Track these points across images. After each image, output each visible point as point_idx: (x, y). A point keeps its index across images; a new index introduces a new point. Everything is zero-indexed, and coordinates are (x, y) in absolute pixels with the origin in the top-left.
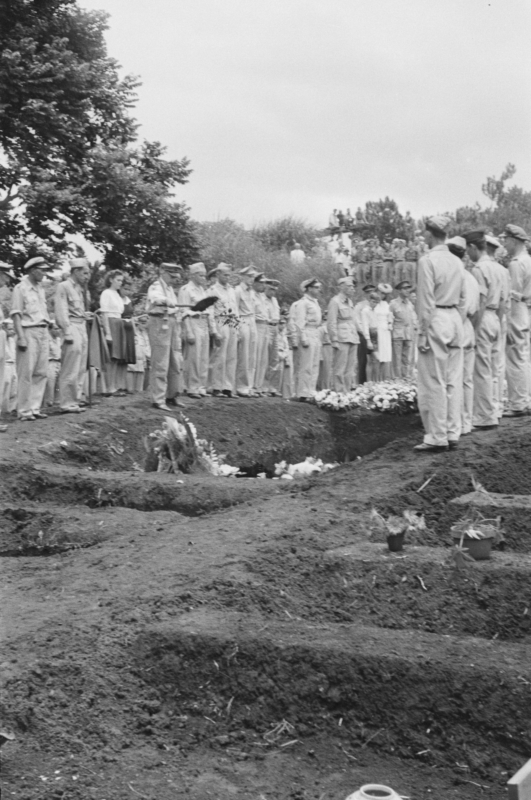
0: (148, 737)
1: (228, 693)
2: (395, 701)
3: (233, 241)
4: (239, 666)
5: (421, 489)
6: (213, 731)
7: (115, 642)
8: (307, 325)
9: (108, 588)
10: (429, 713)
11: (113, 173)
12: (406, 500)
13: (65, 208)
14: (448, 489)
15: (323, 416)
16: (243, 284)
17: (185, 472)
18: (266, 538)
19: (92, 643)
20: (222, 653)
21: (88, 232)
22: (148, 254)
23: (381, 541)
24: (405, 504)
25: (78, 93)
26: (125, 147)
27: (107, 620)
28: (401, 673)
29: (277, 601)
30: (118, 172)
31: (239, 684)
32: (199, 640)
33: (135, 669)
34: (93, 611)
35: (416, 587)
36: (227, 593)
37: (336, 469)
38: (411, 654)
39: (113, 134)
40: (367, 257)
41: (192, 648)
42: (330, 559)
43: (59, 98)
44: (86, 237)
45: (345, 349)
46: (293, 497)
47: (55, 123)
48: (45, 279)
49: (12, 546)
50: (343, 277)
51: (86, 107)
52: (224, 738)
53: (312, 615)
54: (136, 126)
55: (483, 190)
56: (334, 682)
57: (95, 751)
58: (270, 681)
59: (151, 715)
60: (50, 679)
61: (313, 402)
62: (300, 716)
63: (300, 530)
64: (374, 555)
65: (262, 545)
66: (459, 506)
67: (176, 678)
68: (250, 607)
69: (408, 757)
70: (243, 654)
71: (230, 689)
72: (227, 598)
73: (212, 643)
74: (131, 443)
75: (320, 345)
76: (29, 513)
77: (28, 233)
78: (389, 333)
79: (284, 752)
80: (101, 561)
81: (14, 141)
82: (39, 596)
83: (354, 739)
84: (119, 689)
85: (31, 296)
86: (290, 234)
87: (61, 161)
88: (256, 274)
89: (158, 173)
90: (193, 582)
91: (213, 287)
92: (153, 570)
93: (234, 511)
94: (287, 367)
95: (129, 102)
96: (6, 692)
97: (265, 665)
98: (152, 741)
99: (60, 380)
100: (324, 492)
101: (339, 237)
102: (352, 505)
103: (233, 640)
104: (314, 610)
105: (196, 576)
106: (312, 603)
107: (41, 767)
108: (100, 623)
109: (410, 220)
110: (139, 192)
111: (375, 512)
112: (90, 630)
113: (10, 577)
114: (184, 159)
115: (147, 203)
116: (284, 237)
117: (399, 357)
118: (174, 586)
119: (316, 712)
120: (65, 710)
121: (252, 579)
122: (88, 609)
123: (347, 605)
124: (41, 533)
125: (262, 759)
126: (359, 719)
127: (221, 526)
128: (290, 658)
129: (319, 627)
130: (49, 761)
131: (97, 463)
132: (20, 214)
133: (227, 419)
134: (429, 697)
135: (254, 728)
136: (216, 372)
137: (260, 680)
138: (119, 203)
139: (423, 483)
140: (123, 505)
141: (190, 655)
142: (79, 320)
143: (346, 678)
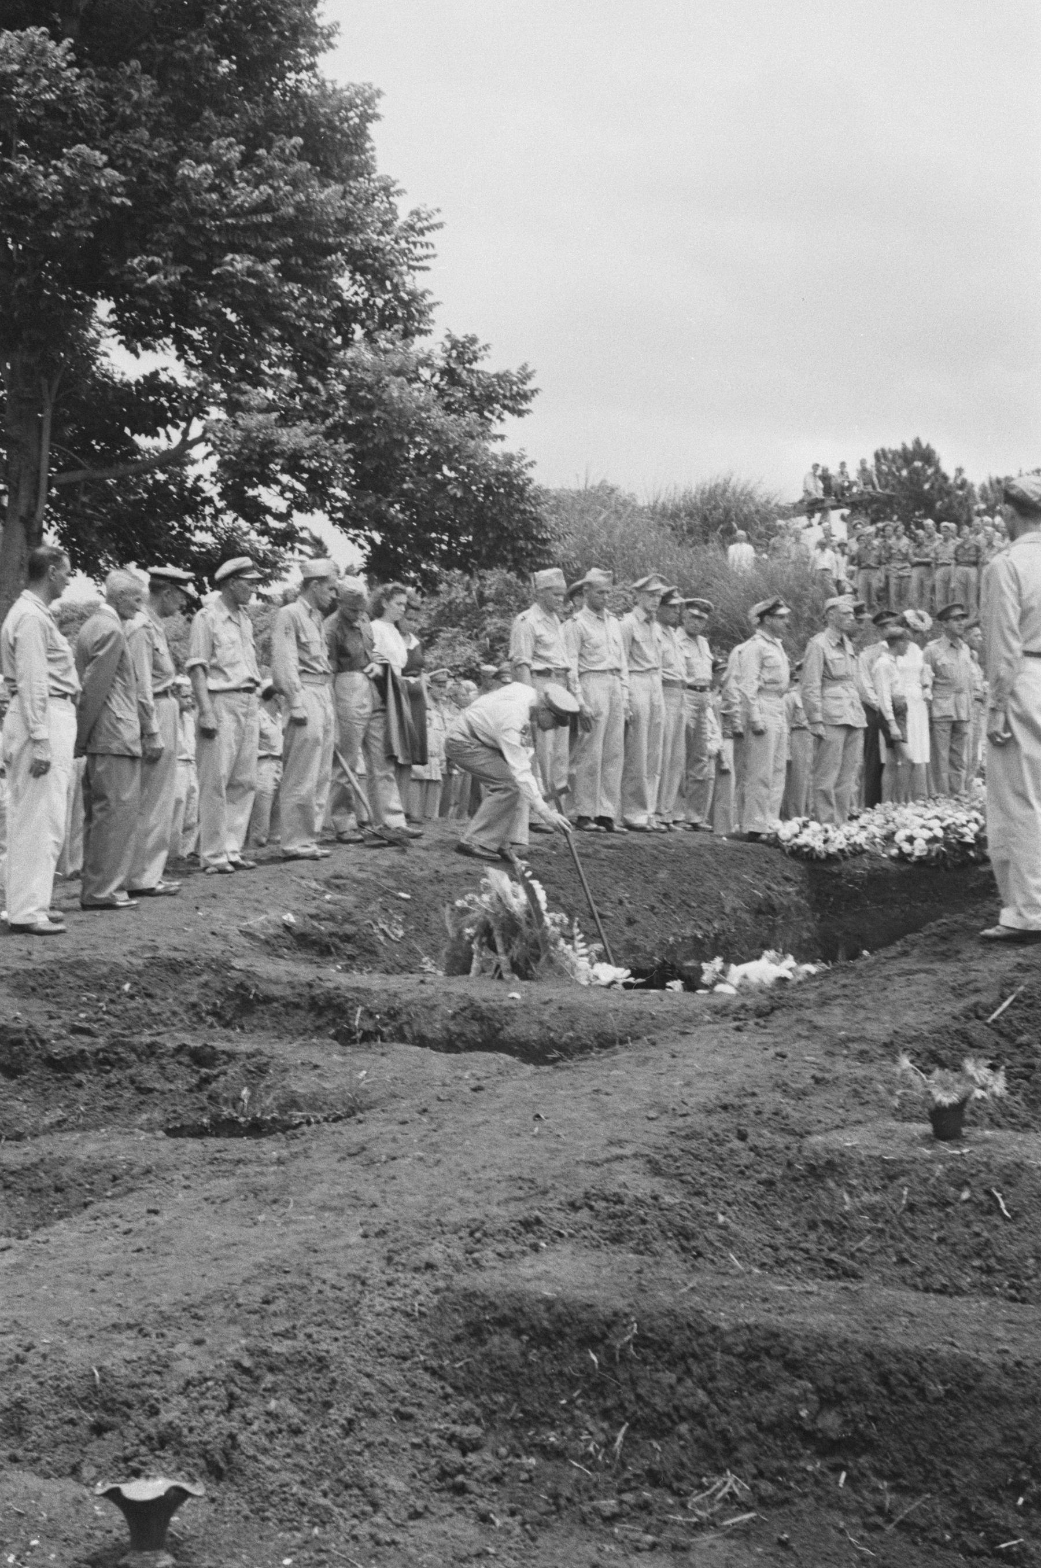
0: (458, 1499)
1: (617, 1416)
2: (953, 1439)
3: (614, 526)
4: (638, 1362)
5: (994, 1016)
6: (586, 1490)
7: (394, 1309)
8: (760, 690)
9: (379, 1203)
10: (1021, 1464)
11: (385, 396)
12: (964, 1036)
13: (293, 464)
15: (794, 869)
16: (637, 610)
17: (524, 977)
18: (685, 1109)
19: (351, 1309)
20: (605, 1336)
21: (335, 510)
22: (450, 552)
23: (919, 1120)
24: (964, 1046)
25: (320, 244)
26: (408, 346)
27: (377, 1264)
28: (964, 1383)
29: (711, 1234)
30: (395, 394)
31: (639, 1397)
32: (560, 1308)
33: (434, 1363)
34: (349, 1248)
35: (989, 1212)
36: (613, 1216)
37: (824, 975)
38: (984, 1345)
39: (386, 321)
40: (879, 557)
41: (546, 1323)
42: (815, 1153)
43: (284, 253)
44: (331, 519)
45: (839, 737)
46: (738, 1029)
47: (277, 301)
48: (254, 601)
49: (191, 1117)
50: (832, 596)
51: (334, 269)
52: (609, 1505)
53: (780, 1263)
54: (431, 307)
56: (828, 1400)
57: (355, 1521)
58: (701, 1394)
59: (464, 1454)
60: (269, 1379)
61: (775, 842)
62: (762, 1466)
63: (754, 1094)
64: (904, 1147)
65: (679, 1122)
67: (515, 1383)
68: (657, 1246)
69: (979, 1554)
70: (646, 1338)
71: (621, 1407)
72: (611, 1227)
73: (584, 1316)
74: (419, 918)
75: (786, 730)
76: (224, 1052)
77: (219, 511)
78: (924, 706)
79: (729, 1536)
80: (364, 1149)
81: (196, 334)
82: (244, 1216)
83: (870, 1514)
84: (403, 1401)
85: (227, 633)
86: (727, 512)
87: (286, 373)
88: (665, 589)
89: (472, 395)
90: (545, 1192)
91: (577, 615)
92: (465, 1167)
93: (623, 1054)
94: (723, 773)
96: (185, 1403)
97: (690, 1361)
98: (468, 1507)
99: (281, 795)
100: (799, 1021)
101: (825, 517)
102: (856, 1047)
103: (627, 1310)
104: (785, 1253)
105: (549, 1183)
106: (780, 1239)
107: (255, 1551)
108: (365, 1270)
109: (963, 485)
110: (436, 432)
111: (905, 1062)
112: (344, 1283)
113: (187, 1178)
114: (524, 368)
115: (450, 453)
116: (715, 518)
117: (945, 753)
118: (507, 1201)
119: (792, 1458)
120: (298, 1440)
121: (660, 1190)
122: (341, 1242)
123: (851, 1246)
124: (245, 1092)
125: (685, 1549)
126: (880, 1474)
127: (596, 1084)
128: (741, 1349)
129: (798, 1287)
130: (269, 1538)
131: (352, 958)
132: (207, 476)
133: (604, 874)
134: (1022, 1432)
135: (669, 1487)
136: (583, 782)
137: (681, 1390)
138: (397, 454)
139: (1000, 1004)
140: (403, 1039)
141: (542, 1338)
142: (318, 679)
143: (853, 1391)
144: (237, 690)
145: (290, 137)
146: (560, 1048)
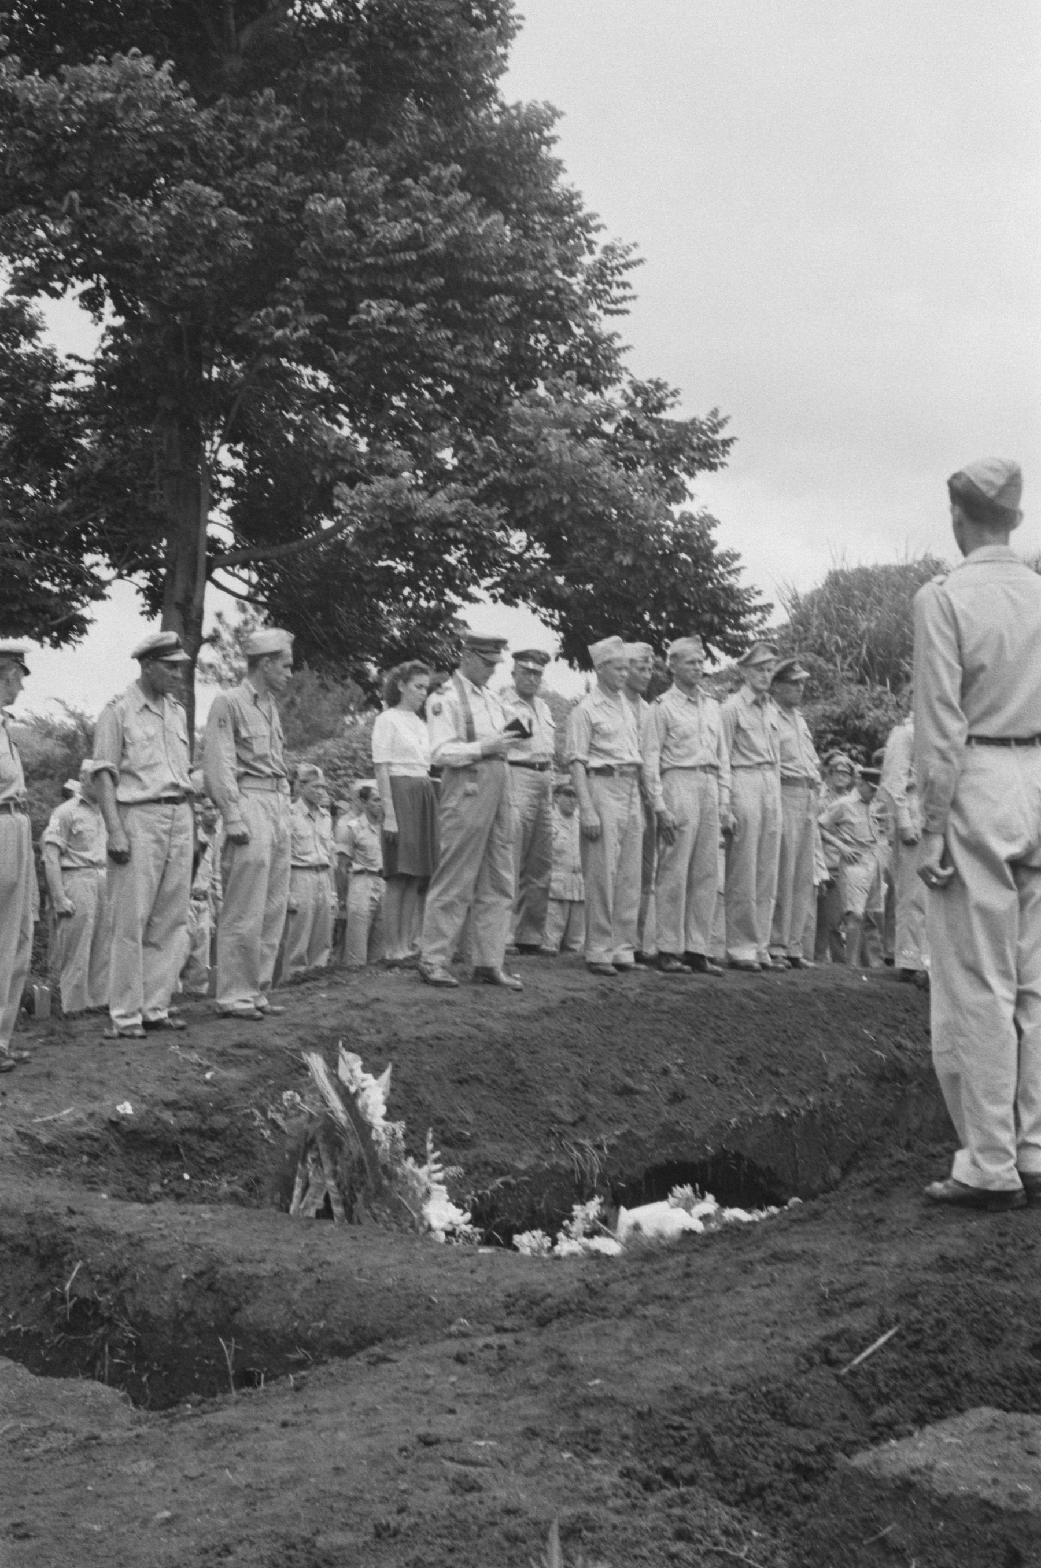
14: (938, 1371)
30: (553, 448)
43: (438, 295)
54: (617, 352)
66: (874, 1483)
95: (615, 302)
114: (714, 413)
144: (158, 801)
145: (446, 165)
146: (308, 1346)
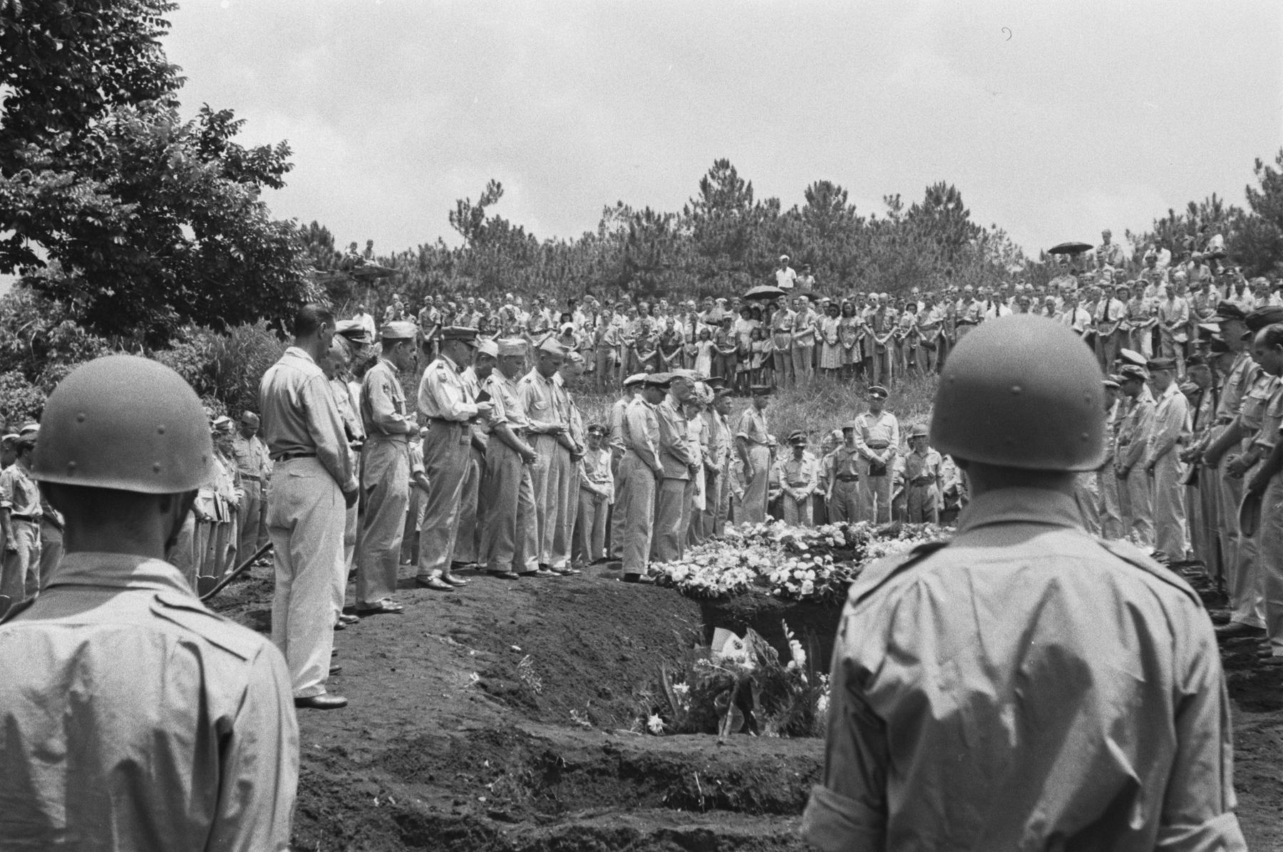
55: (451, 220)
114: (284, 144)
